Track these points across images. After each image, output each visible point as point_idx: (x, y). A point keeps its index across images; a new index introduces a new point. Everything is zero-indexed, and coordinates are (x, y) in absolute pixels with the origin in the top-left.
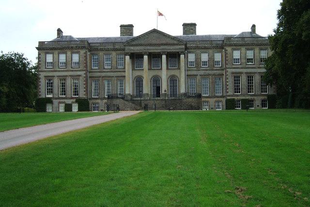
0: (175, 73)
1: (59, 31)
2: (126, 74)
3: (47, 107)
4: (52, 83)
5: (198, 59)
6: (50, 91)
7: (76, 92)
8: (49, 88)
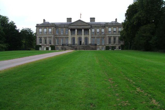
0: (87, 36)
6: (41, 43)
7: (50, 43)
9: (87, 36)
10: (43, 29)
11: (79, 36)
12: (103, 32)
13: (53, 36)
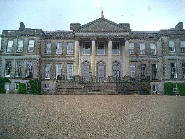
0: (104, 59)
1: (22, 25)
2: (128, 60)
3: (6, 86)
4: (10, 65)
5: (137, 48)
6: (9, 72)
7: (30, 74)
8: (8, 69)
9: (104, 59)
10: (177, 41)
11: (98, 59)
12: (143, 50)
13: (37, 57)
